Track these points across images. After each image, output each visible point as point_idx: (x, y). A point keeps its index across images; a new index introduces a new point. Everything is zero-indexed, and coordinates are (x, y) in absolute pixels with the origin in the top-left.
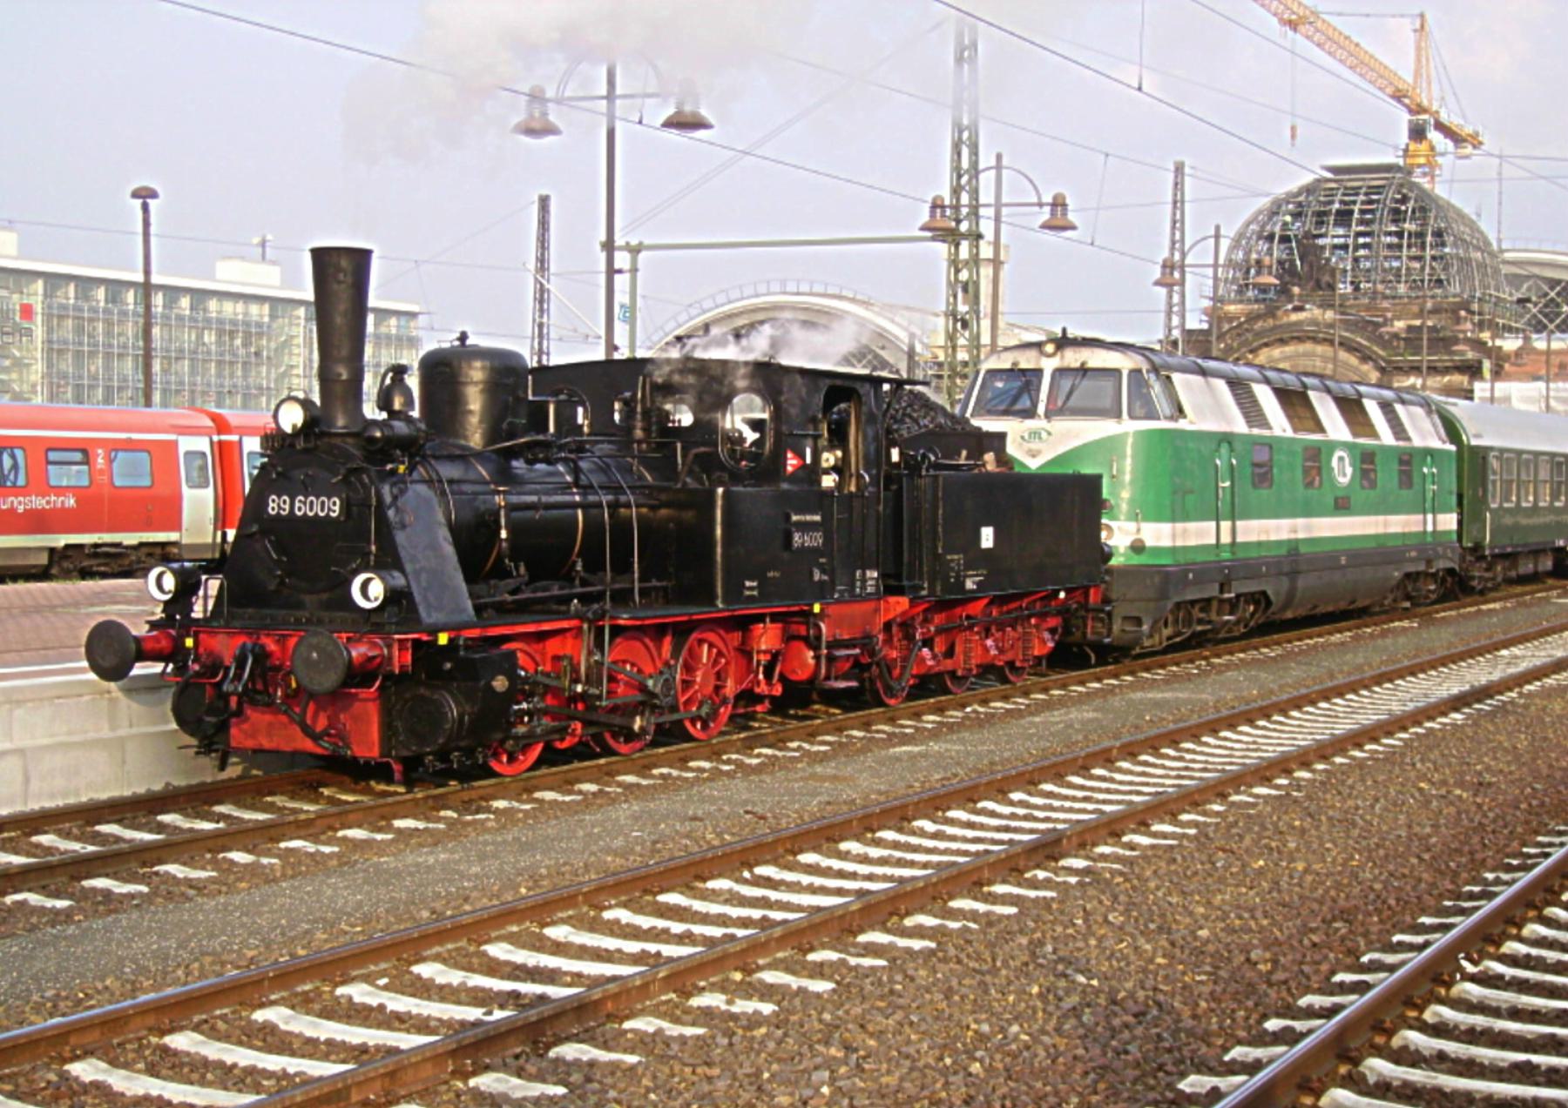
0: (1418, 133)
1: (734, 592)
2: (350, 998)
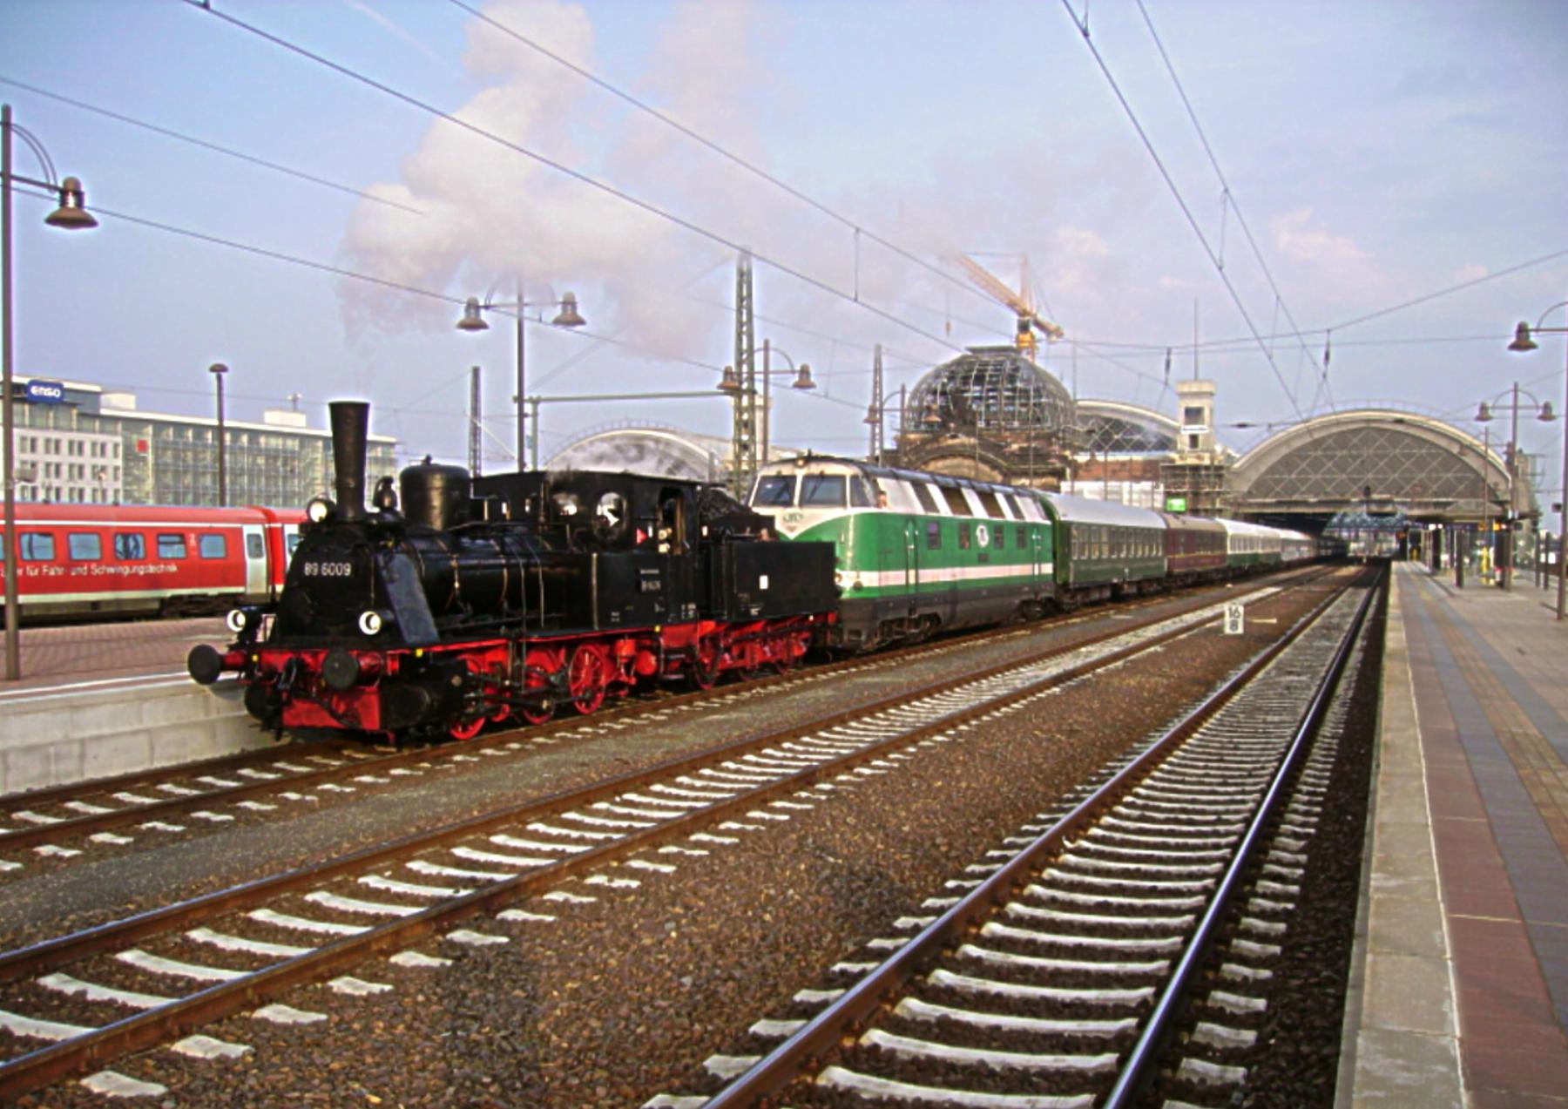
0: (1024, 328)
1: (605, 620)
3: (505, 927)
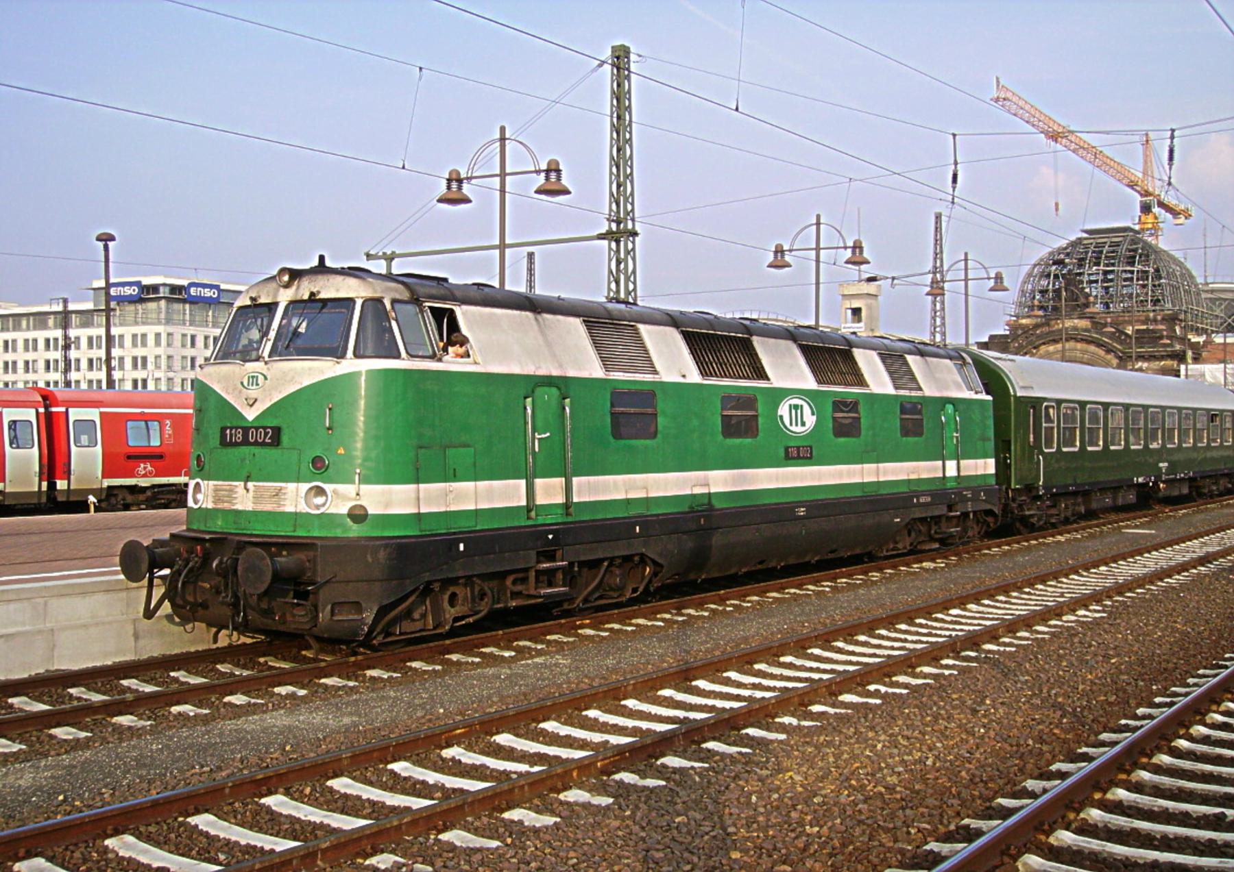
0: (1146, 209)
2: (197, 826)
3: (662, 772)
